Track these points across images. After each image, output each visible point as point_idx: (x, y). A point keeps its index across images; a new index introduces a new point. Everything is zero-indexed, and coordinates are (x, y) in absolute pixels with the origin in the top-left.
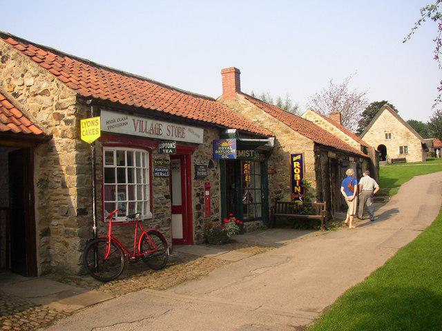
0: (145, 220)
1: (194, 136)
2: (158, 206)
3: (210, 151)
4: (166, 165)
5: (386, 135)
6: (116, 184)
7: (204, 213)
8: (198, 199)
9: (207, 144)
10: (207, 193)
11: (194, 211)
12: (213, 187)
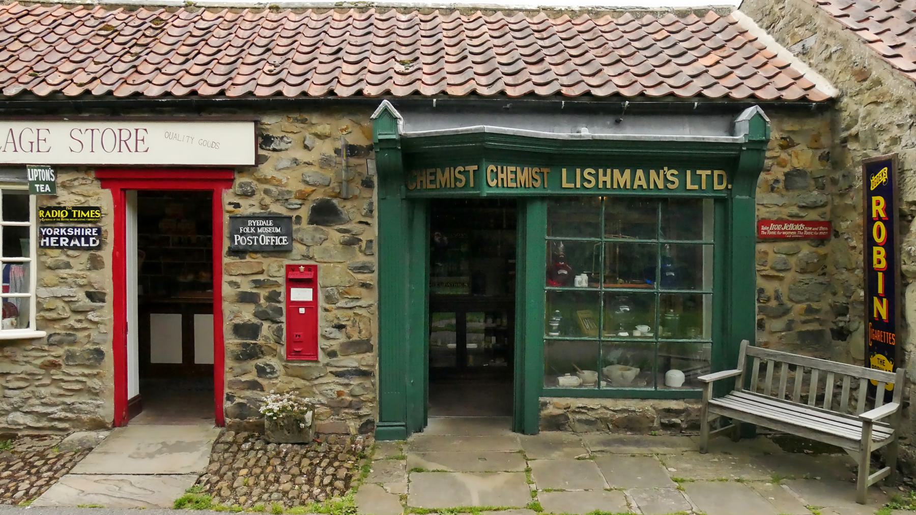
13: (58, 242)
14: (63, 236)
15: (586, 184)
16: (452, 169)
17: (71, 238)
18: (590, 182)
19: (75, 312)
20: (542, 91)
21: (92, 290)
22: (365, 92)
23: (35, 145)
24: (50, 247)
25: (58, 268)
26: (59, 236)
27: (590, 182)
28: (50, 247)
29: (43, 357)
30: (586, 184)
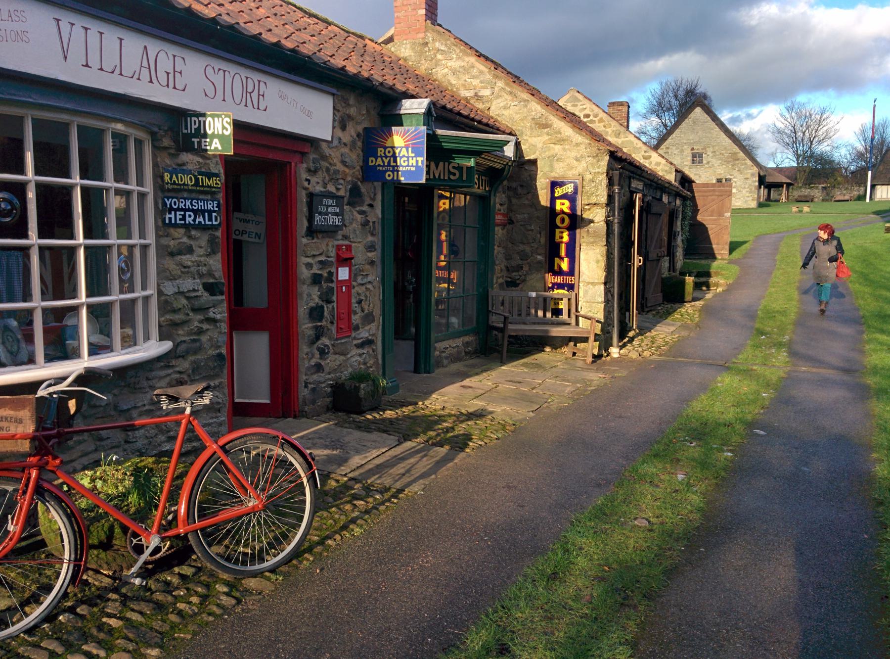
0: (58, 419)
1: (306, 113)
2: (178, 317)
3: (354, 157)
4: (210, 193)
5: (694, 156)
6: (33, 239)
7: (334, 329)
8: (315, 292)
9: (346, 137)
10: (343, 273)
11: (306, 327)
12: (360, 255)
13: (184, 218)
14: (189, 210)
15: (452, 177)
16: (446, 164)
17: (196, 212)
18: (454, 174)
19: (195, 310)
20: (266, 36)
21: (211, 281)
22: (263, 36)
23: (171, 76)
24: (176, 226)
25: (180, 253)
26: (185, 210)
27: (454, 174)
28: (176, 226)
29: (169, 375)
30: (452, 177)
